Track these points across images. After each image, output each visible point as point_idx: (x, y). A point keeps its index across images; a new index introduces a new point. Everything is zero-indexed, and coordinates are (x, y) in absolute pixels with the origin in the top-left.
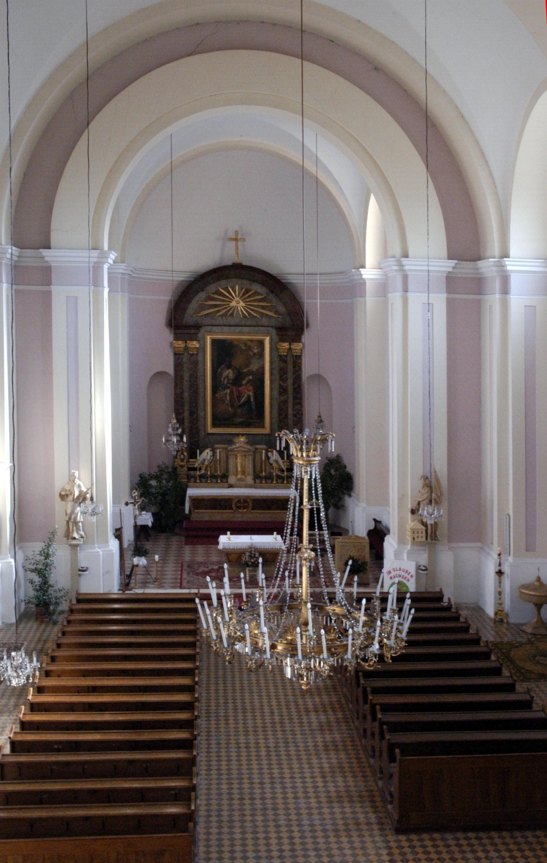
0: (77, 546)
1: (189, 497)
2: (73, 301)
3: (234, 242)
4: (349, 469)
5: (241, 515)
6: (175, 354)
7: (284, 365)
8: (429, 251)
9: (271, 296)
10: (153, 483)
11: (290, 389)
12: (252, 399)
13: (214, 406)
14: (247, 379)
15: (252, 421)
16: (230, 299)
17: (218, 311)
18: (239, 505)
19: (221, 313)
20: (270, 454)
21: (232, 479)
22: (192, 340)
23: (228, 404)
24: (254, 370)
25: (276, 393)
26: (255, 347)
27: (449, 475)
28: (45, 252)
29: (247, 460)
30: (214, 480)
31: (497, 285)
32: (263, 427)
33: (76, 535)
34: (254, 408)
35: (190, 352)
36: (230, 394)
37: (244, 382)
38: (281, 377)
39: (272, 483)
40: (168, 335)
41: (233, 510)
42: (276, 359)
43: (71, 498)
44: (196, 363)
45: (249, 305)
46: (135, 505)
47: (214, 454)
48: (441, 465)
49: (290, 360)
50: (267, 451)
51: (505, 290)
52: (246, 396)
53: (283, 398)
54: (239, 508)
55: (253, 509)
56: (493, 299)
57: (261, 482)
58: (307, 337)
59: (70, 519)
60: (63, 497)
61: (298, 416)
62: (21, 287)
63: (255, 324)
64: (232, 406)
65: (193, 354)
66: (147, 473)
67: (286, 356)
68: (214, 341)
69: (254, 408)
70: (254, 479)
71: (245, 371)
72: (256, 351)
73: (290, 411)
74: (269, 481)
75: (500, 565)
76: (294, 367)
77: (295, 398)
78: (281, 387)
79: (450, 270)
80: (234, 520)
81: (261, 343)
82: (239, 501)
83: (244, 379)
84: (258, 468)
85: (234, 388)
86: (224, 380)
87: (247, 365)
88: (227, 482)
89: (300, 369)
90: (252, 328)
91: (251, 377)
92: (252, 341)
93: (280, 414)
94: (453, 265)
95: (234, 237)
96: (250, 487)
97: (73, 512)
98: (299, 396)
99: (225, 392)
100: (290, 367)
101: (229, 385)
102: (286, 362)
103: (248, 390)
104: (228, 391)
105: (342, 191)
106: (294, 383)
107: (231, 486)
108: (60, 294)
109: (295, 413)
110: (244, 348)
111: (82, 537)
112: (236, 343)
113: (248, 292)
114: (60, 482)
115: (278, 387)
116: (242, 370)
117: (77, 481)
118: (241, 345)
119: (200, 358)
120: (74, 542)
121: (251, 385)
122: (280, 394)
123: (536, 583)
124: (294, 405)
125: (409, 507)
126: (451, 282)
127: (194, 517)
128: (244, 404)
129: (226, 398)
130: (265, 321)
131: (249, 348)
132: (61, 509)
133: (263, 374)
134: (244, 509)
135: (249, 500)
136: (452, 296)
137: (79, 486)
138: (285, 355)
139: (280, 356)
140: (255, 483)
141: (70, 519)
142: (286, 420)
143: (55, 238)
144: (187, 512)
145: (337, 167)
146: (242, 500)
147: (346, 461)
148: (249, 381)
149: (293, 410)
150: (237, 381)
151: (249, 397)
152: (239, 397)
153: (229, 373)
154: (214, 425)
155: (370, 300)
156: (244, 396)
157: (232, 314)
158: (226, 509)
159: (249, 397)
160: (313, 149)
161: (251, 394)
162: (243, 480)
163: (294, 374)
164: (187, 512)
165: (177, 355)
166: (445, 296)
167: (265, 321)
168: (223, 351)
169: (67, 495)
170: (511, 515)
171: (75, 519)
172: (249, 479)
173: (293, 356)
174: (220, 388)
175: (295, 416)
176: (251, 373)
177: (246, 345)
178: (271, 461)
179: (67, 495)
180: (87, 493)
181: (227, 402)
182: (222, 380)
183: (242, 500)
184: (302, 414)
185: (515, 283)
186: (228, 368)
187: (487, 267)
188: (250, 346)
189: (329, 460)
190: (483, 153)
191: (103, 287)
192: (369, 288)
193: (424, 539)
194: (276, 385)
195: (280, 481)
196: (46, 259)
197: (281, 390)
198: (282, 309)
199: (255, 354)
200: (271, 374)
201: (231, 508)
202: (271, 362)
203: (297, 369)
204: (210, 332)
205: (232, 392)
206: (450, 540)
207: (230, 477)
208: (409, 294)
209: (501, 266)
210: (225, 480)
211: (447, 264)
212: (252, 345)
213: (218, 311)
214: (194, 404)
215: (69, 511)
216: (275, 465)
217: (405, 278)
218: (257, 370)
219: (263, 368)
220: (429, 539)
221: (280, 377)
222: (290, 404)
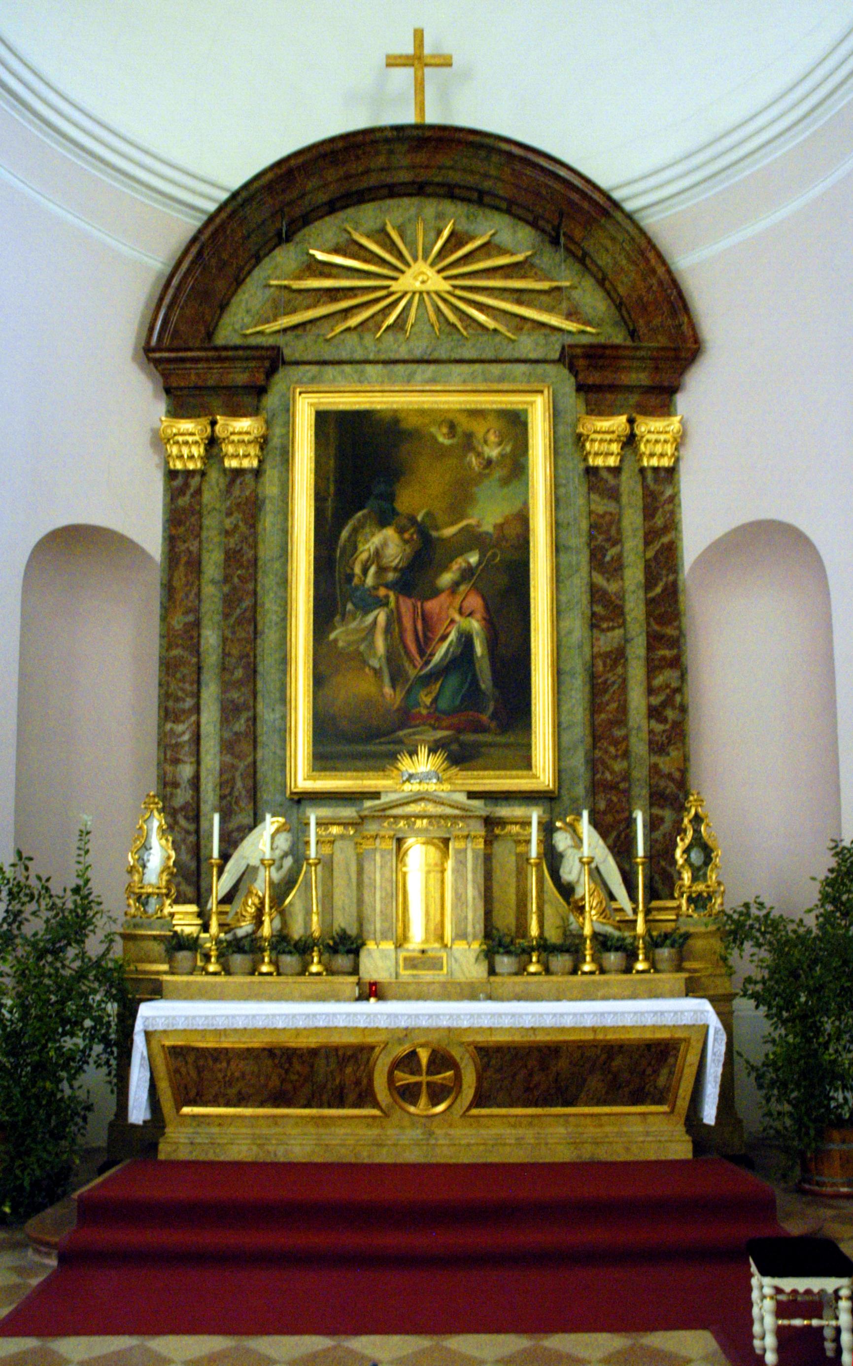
1: (148, 1035)
3: (409, 72)
5: (417, 1133)
6: (172, 474)
7: (612, 507)
9: (549, 258)
11: (635, 608)
12: (479, 649)
14: (459, 563)
15: (481, 737)
16: (396, 269)
17: (346, 313)
18: (404, 1078)
19: (353, 322)
20: (562, 841)
21: (378, 960)
22: (236, 412)
23: (377, 672)
24: (488, 527)
25: (577, 625)
26: (492, 438)
29: (450, 864)
30: (289, 961)
32: (526, 763)
34: (486, 683)
35: (227, 463)
36: (388, 630)
37: (447, 578)
38: (596, 558)
40: (139, 400)
41: (376, 1104)
42: (577, 486)
44: (252, 509)
45: (463, 288)
47: (297, 851)
49: (630, 488)
50: (548, 830)
52: (452, 636)
53: (608, 641)
54: (409, 1094)
55: (480, 1100)
57: (522, 970)
58: (703, 392)
61: (670, 714)
63: (489, 354)
65: (238, 472)
67: (616, 471)
68: (322, 418)
69: (486, 683)
70: (489, 955)
71: (449, 531)
72: (493, 452)
73: (637, 701)
74: (561, 962)
76: (649, 512)
77: (654, 640)
78: (596, 594)
80: (384, 1157)
81: (516, 423)
82: (409, 1061)
83: (445, 568)
84: (506, 894)
85: (406, 606)
86: (365, 571)
87: (457, 510)
88: (355, 971)
89: (672, 525)
90: (477, 366)
91: (474, 559)
92: (476, 414)
93: (594, 708)
95: (410, 50)
96: (470, 992)
98: (669, 631)
99: (370, 618)
100: (632, 520)
101: (382, 592)
102: (614, 494)
103: (461, 612)
104: (381, 616)
107: (373, 991)
109: (656, 701)
110: (447, 442)
112: (411, 423)
113: (461, 244)
115: (585, 599)
116: (437, 529)
118: (433, 430)
119: (270, 488)
121: (475, 588)
122: (594, 623)
124: (652, 667)
127: (178, 1143)
129: (372, 645)
130: (528, 346)
131: (468, 443)
133: (523, 544)
134: (435, 1101)
135: (456, 1053)
138: (609, 469)
139: (591, 472)
140: (492, 972)
142: (619, 733)
144: (138, 1112)
146: (424, 1056)
148: (468, 573)
149: (651, 691)
150: (416, 575)
151: (466, 640)
152: (424, 647)
153: (385, 544)
154: (324, 759)
156: (444, 638)
157: (399, 325)
158: (341, 1104)
159: (466, 640)
161: (475, 625)
162: (436, 964)
163: (647, 544)
164: (138, 1112)
165: (178, 483)
167: (528, 346)
168: (365, 461)
172: (465, 959)
173: (642, 470)
174: (350, 606)
175: (654, 713)
176: (472, 539)
177: (452, 427)
178: (571, 871)
181: (375, 663)
182: (357, 570)
183: (424, 1056)
184: (683, 709)
186: (383, 523)
188: (469, 436)
194: (578, 586)
195: (613, 958)
197: (598, 609)
198: (593, 301)
199: (489, 462)
200: (558, 548)
201: (366, 1097)
202: (558, 502)
203: (659, 521)
204: (313, 385)
205: (395, 619)
207: (371, 945)
210: (343, 961)
212: (479, 428)
213: (346, 313)
214: (239, 673)
216: (585, 888)
218: (500, 527)
219: (523, 519)
221: (593, 556)
222: (636, 671)
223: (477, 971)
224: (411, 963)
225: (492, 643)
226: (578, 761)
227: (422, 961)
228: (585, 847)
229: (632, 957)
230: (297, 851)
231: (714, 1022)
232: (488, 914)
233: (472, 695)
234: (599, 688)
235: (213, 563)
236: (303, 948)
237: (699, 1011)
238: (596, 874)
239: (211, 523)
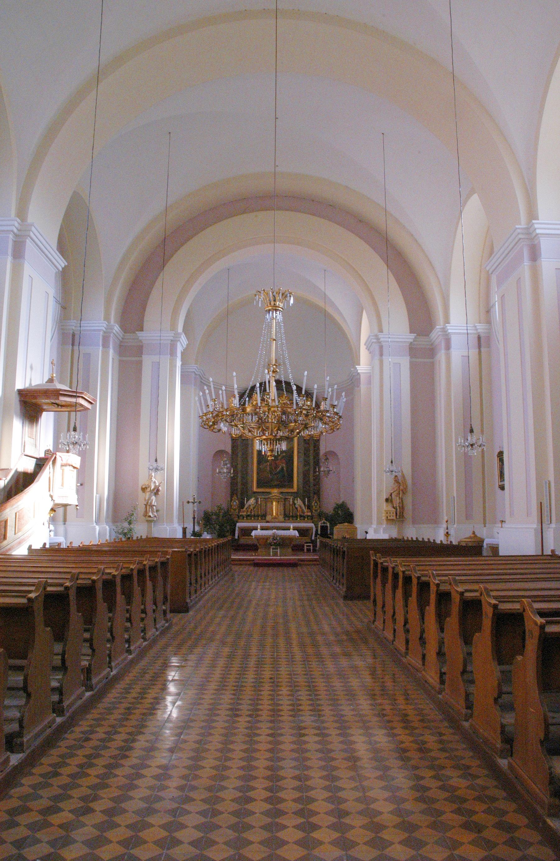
0: (151, 521)
2: (157, 366)
4: (351, 510)
8: (398, 327)
10: (214, 517)
13: (258, 473)
20: (296, 502)
21: (268, 518)
27: (413, 475)
28: (139, 334)
31: (443, 345)
32: (293, 487)
33: (151, 514)
39: (297, 520)
43: (149, 490)
46: (194, 504)
47: (257, 502)
48: (407, 470)
50: (294, 500)
51: (448, 347)
53: (307, 468)
56: (441, 356)
59: (147, 503)
60: (144, 489)
62: (124, 359)
64: (271, 473)
66: (210, 511)
74: (295, 519)
75: (447, 529)
76: (314, 447)
79: (412, 340)
89: (318, 449)
94: (413, 337)
97: (149, 499)
100: (312, 447)
105: (345, 321)
106: (314, 458)
107: (268, 522)
108: (147, 361)
111: (155, 517)
114: (142, 481)
117: (154, 479)
120: (150, 519)
122: (305, 465)
123: (473, 535)
125: (385, 498)
126: (413, 351)
128: (279, 473)
132: (142, 498)
136: (414, 360)
137: (155, 482)
141: (147, 503)
143: (146, 325)
144: (236, 537)
145: (339, 298)
147: (350, 506)
151: (283, 468)
154: (259, 486)
155: (363, 387)
159: (283, 468)
160: (322, 288)
161: (284, 465)
166: (409, 358)
169: (146, 488)
170: (455, 496)
171: (151, 503)
172: (281, 518)
175: (314, 480)
178: (297, 506)
179: (146, 488)
180: (159, 486)
185: (454, 341)
187: (435, 334)
189: (337, 505)
190: (430, 263)
191: (176, 356)
192: (363, 379)
193: (394, 518)
194: (302, 459)
196: (140, 338)
200: (298, 452)
202: (298, 445)
206: (414, 522)
208: (384, 357)
209: (444, 330)
211: (409, 337)
215: (147, 499)
216: (299, 508)
217: (381, 348)
220: (398, 517)
222: (312, 472)
223: (283, 520)
224: (273, 518)
225: (287, 468)
226: (301, 486)
227: (275, 518)
228: (299, 502)
229: (244, 517)
230: (257, 502)
231: (314, 526)
232: (285, 512)
233: (284, 476)
234: (305, 475)
235: (240, 454)
236: (258, 516)
237: (311, 525)
238: (300, 507)
239: (240, 448)
